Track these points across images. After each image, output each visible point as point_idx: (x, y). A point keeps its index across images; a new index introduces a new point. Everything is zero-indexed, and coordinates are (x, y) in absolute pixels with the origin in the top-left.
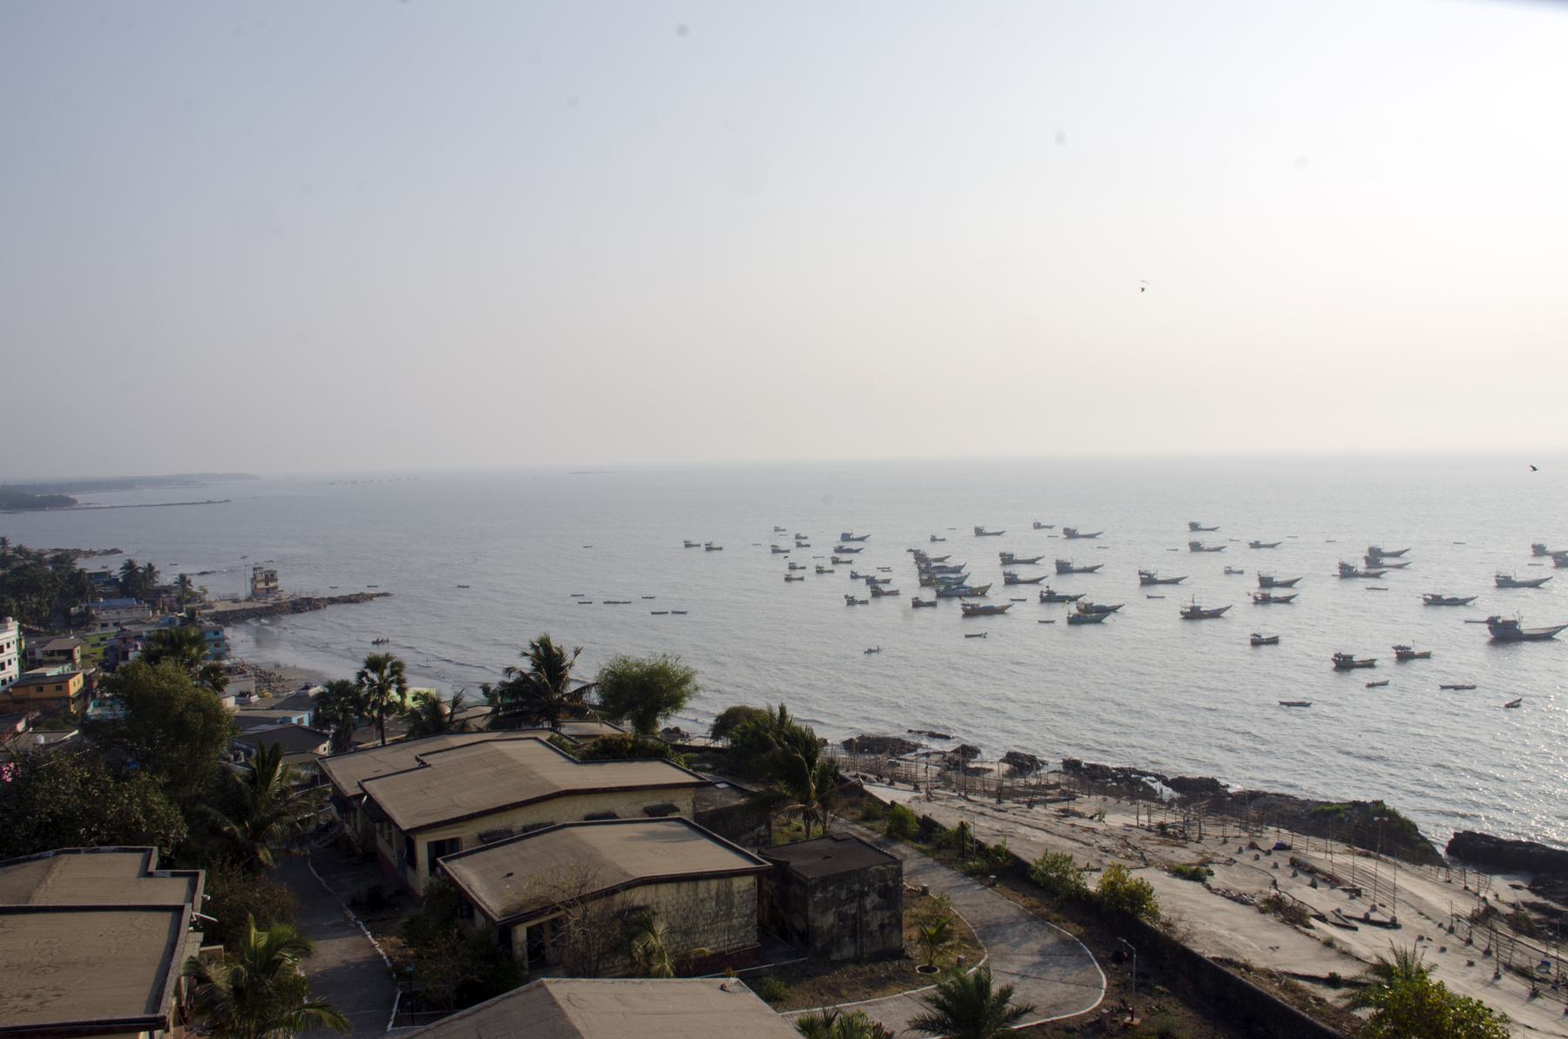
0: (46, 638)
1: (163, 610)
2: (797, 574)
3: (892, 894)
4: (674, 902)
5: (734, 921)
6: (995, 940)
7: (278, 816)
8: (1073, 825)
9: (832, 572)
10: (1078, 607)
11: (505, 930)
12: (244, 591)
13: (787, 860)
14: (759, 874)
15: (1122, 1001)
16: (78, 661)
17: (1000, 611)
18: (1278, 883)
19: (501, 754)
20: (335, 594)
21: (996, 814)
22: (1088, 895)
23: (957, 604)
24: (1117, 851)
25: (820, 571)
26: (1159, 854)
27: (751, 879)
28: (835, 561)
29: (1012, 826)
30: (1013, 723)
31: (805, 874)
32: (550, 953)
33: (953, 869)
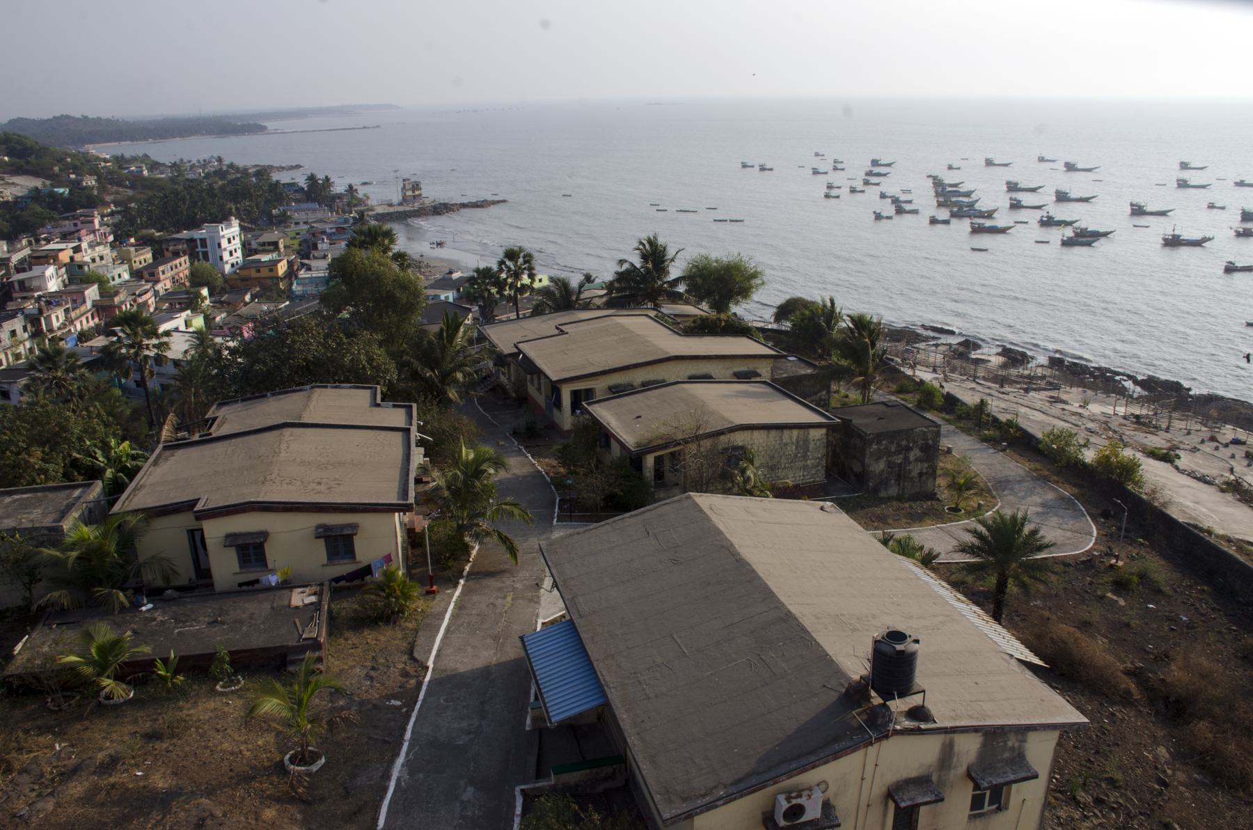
0: (257, 233)
1: (337, 213)
2: (834, 192)
3: (931, 451)
4: (764, 444)
5: (809, 462)
6: (1005, 493)
7: (460, 367)
8: (1063, 409)
9: (863, 191)
10: (1074, 231)
11: (635, 460)
12: (396, 197)
13: (850, 418)
14: (831, 428)
15: (1109, 547)
16: (282, 250)
17: (1003, 231)
18: (1235, 470)
19: (622, 326)
20: (465, 201)
21: (1001, 396)
22: (1084, 465)
23: (965, 225)
24: (1100, 433)
25: (853, 191)
26: (1135, 438)
27: (824, 431)
28: (866, 183)
29: (1015, 406)
30: (994, 331)
31: (864, 429)
32: (669, 476)
33: (971, 435)
